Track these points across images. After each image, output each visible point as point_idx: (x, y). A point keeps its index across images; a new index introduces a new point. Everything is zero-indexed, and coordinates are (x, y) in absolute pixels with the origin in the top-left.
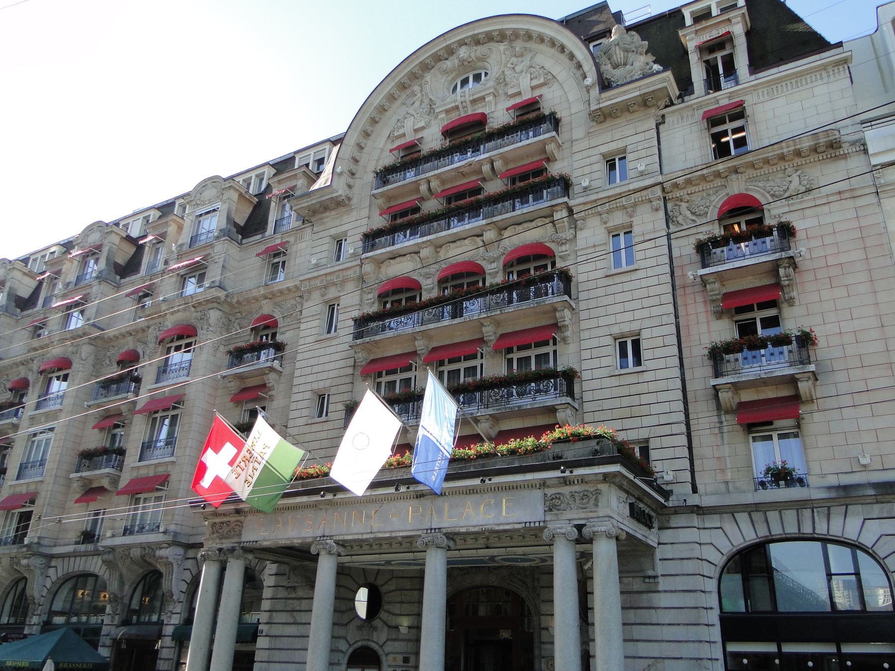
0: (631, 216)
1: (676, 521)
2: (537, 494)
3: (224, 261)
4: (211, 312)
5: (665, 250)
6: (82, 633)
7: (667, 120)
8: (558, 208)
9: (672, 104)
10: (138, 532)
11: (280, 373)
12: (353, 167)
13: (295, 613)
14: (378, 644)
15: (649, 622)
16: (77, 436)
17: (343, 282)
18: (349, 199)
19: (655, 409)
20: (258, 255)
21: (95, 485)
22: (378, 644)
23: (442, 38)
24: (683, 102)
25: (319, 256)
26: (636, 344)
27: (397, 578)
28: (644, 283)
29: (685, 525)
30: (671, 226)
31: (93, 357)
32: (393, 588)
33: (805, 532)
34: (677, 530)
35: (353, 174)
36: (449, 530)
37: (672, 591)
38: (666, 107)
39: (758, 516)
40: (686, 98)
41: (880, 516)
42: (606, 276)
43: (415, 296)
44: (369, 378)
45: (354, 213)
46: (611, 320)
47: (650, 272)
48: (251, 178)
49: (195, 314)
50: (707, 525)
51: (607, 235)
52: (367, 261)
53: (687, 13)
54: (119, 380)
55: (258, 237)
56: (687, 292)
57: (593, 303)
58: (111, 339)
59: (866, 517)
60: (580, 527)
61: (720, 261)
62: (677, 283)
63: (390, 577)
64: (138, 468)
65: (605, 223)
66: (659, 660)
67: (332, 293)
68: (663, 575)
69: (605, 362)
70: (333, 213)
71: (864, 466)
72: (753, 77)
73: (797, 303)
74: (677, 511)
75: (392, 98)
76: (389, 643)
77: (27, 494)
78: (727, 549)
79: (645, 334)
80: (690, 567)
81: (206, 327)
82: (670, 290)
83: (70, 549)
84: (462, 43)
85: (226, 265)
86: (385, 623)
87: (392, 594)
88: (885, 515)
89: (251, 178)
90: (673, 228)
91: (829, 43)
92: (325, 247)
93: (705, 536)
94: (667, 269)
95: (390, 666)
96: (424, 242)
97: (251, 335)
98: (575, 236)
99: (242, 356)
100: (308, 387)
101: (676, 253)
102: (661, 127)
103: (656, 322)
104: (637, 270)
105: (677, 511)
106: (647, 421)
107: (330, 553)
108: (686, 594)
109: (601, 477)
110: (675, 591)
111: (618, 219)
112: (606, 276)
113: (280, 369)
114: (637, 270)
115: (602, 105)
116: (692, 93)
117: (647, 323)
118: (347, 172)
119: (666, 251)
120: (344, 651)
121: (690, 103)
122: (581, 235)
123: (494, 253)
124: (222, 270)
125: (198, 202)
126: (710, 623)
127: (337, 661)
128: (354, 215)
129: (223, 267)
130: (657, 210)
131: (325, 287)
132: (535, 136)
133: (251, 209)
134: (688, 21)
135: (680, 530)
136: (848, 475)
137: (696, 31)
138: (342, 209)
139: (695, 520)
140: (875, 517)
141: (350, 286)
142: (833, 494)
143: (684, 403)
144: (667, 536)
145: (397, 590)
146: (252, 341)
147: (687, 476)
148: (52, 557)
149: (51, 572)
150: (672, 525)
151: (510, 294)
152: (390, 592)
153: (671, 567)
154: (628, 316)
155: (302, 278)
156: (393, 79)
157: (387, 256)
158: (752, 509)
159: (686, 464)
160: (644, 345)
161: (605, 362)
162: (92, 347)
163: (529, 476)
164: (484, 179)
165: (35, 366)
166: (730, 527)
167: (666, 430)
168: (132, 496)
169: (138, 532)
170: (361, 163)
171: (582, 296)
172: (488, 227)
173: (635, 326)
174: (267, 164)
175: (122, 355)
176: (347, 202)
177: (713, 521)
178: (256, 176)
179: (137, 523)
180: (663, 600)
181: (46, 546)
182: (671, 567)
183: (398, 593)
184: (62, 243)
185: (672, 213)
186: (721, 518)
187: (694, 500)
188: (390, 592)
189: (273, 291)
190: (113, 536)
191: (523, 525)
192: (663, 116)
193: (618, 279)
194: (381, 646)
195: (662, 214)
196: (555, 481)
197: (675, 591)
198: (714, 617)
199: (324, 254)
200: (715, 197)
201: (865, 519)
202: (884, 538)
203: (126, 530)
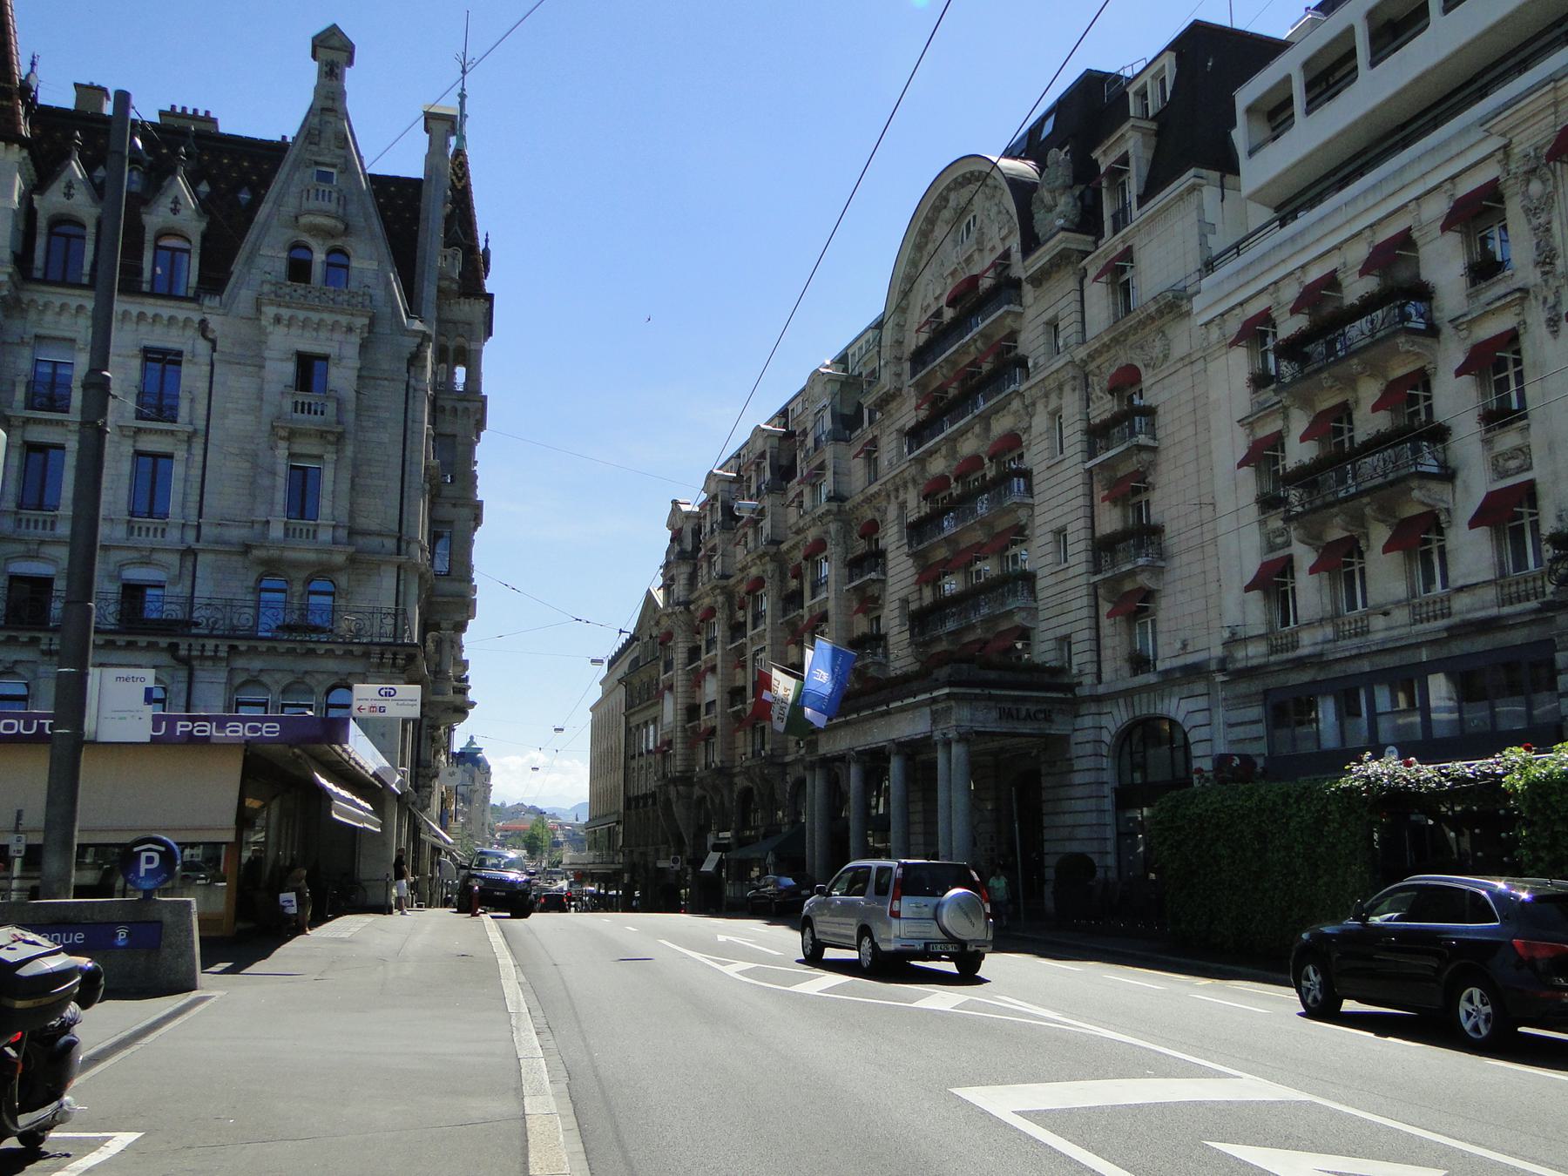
2: (927, 710)
3: (834, 467)
8: (1013, 396)
11: (1154, 450)
17: (1060, 388)
23: (933, 188)
54: (1116, 420)
75: (914, 263)
84: (949, 189)
99: (1108, 432)
113: (1151, 443)
115: (1028, 274)
132: (983, 321)
137: (1104, 152)
141: (910, 486)
146: (1116, 409)
156: (909, 242)
158: (1128, 694)
162: (775, 564)
164: (730, 541)
168: (753, 727)
172: (976, 421)
178: (1153, 77)
184: (873, 326)
187: (1101, 690)
189: (1148, 315)
196: (942, 698)
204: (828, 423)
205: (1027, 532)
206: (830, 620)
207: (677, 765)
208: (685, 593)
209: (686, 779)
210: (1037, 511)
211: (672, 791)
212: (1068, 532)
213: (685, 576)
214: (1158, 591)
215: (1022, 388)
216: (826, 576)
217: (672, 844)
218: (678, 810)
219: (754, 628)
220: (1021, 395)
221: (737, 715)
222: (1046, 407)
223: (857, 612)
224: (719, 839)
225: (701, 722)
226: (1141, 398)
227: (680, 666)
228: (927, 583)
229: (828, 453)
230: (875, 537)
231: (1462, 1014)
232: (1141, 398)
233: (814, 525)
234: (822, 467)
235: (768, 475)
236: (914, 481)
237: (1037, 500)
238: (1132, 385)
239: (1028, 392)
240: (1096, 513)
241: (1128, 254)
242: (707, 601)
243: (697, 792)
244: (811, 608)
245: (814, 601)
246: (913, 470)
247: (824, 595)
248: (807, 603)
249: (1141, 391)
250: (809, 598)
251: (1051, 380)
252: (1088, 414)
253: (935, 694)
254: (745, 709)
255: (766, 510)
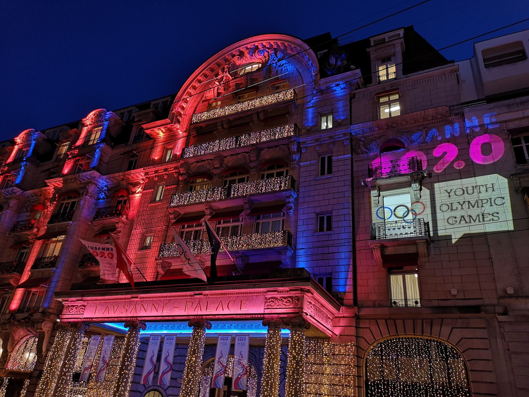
6: (88, 161)
7: (356, 96)
9: (359, 88)
10: (26, 311)
21: (6, 282)
22: (163, 389)
24: (366, 87)
26: (329, 219)
38: (356, 89)
40: (368, 85)
48: (124, 113)
53: (372, 40)
56: (359, 191)
58: (28, 197)
59: (453, 327)
61: (269, 148)
62: (355, 186)
71: (454, 296)
72: (404, 76)
76: (170, 388)
79: (334, 213)
81: (85, 193)
82: (350, 189)
89: (124, 113)
91: (447, 60)
94: (349, 177)
101: (355, 169)
102: (353, 100)
116: (371, 82)
119: (350, 167)
120: (142, 392)
121: (369, 88)
134: (372, 43)
140: (459, 327)
143: (353, 253)
151: (200, 154)
160: (334, 219)
169: (26, 311)
173: (329, 208)
174: (8, 141)
178: (128, 112)
179: (27, 306)
185: (355, 147)
192: (354, 94)
194: (165, 390)
200: (379, 140)
201: (453, 328)
202: (464, 340)
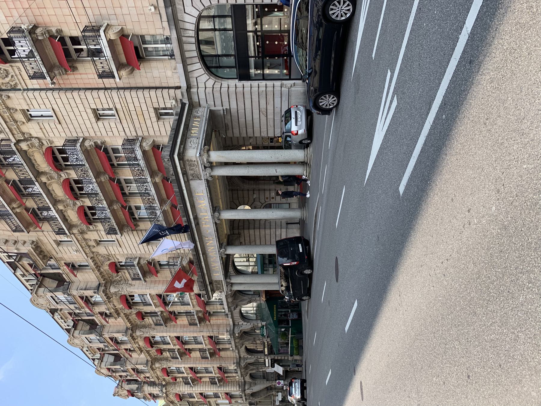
0: (16, 110)
1: (195, 98)
3: (81, 289)
4: (111, 291)
5: (37, 93)
8: (19, 147)
11: (140, 258)
12: (11, 243)
13: (251, 241)
14: (261, 206)
15: (244, 113)
16: (181, 327)
17: (85, 239)
18: (33, 242)
19: (137, 104)
20: (76, 276)
22: (261, 206)
25: (72, 251)
27: (233, 199)
28: (61, 105)
29: (197, 95)
30: (18, 88)
31: (141, 329)
32: (237, 201)
33: (194, 41)
34: (200, 99)
35: (16, 242)
36: (212, 212)
37: (229, 103)
39: (189, 61)
41: (182, 5)
42: (121, 247)
43: (57, 149)
44: (116, 171)
45: (41, 238)
46: (88, 122)
47: (53, 102)
49: (114, 298)
50: (196, 84)
51: (32, 122)
52: (71, 232)
55: (64, 276)
57: (79, 130)
59: (184, 12)
60: (205, 167)
63: (233, 203)
64: (193, 305)
65: (24, 123)
66: (260, 110)
67: (92, 243)
68: (222, 106)
69: (113, 125)
70: (43, 247)
73: (59, 28)
74: (190, 98)
77: (209, 340)
78: (206, 77)
80: (217, 95)
83: (231, 320)
85: (84, 288)
86: (253, 203)
87: (240, 201)
88: (182, 3)
90: (19, 87)
92: (65, 248)
93: (202, 85)
95: (270, 200)
96: (55, 209)
97: (121, 272)
98: (36, 138)
100: (95, 125)
103: (85, 102)
104: (53, 109)
105: (190, 98)
106: (144, 108)
107: (226, 250)
108: (230, 97)
109: (181, 161)
110: (229, 101)
111: (20, 117)
112: (60, 123)
113: (137, 259)
114: (53, 109)
117: (87, 105)
118: (16, 246)
122: (34, 135)
123: (55, 175)
124: (87, 290)
125: (48, 305)
126: (242, 86)
127: (269, 224)
128: (43, 238)
129: (85, 290)
130: (9, 97)
131: (89, 246)
133: (46, 279)
135: (200, 98)
136: (162, 16)
138: (40, 244)
139: (194, 90)
140: (183, 8)
141: (86, 236)
142: (173, 27)
144: (203, 103)
145: (238, 200)
147: (172, 91)
148: (234, 325)
149: (240, 323)
150: (198, 101)
152: (239, 202)
153: (218, 102)
154: (84, 114)
155: (86, 257)
157: (66, 223)
159: (165, 91)
161: (113, 125)
163: (184, 188)
165: (128, 311)
166: (196, 74)
167: (148, 100)
170: (7, 238)
171: (75, 135)
175: (138, 318)
176: (35, 243)
177: (193, 82)
180: (234, 106)
181: (230, 328)
182: (218, 102)
183: (239, 199)
184: (13, 271)
186: (192, 77)
187: (184, 85)
188: (239, 202)
189: (96, 268)
190: (224, 309)
191: (207, 187)
193: (61, 118)
195: (11, 94)
197: (229, 101)
198: (240, 84)
199: (70, 248)
203: (221, 304)
204: (93, 337)
205: (99, 142)
206: (178, 335)
207: (235, 390)
208: (157, 388)
209: (243, 385)
210: (87, 135)
211: (248, 392)
212: (95, 108)
213: (149, 387)
214: (154, 141)
215: (14, 141)
216: (176, 368)
217: (271, 393)
218: (256, 389)
219: (194, 397)
220: (18, 142)
221: (220, 381)
222: (94, 247)
223: (176, 323)
224: (269, 366)
225: (216, 376)
226: (122, 262)
227: (191, 389)
228: (137, 226)
229: (129, 367)
230: (144, 314)
231: (343, 18)
232: (122, 262)
233: (138, 342)
234: (111, 339)
235: (118, 367)
236: (82, 232)
237: (81, 135)
238: (116, 265)
239: (16, 136)
240: (84, 87)
241: (67, 265)
242: (159, 373)
243: (248, 379)
244: (188, 374)
245: (185, 373)
246: (75, 231)
247: (183, 369)
248: (185, 375)
249: (119, 262)
250: (183, 374)
251: (79, 237)
252: (24, 90)
253: (208, 283)
254: (217, 377)
255: (110, 336)
